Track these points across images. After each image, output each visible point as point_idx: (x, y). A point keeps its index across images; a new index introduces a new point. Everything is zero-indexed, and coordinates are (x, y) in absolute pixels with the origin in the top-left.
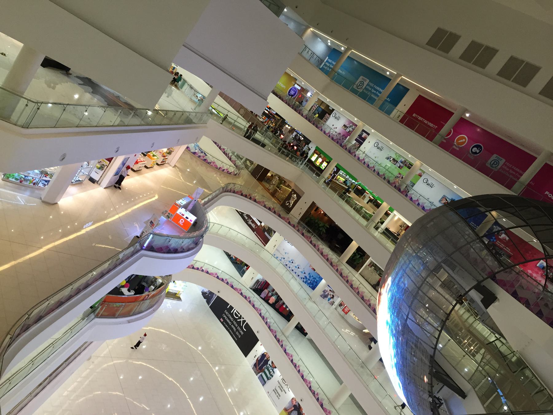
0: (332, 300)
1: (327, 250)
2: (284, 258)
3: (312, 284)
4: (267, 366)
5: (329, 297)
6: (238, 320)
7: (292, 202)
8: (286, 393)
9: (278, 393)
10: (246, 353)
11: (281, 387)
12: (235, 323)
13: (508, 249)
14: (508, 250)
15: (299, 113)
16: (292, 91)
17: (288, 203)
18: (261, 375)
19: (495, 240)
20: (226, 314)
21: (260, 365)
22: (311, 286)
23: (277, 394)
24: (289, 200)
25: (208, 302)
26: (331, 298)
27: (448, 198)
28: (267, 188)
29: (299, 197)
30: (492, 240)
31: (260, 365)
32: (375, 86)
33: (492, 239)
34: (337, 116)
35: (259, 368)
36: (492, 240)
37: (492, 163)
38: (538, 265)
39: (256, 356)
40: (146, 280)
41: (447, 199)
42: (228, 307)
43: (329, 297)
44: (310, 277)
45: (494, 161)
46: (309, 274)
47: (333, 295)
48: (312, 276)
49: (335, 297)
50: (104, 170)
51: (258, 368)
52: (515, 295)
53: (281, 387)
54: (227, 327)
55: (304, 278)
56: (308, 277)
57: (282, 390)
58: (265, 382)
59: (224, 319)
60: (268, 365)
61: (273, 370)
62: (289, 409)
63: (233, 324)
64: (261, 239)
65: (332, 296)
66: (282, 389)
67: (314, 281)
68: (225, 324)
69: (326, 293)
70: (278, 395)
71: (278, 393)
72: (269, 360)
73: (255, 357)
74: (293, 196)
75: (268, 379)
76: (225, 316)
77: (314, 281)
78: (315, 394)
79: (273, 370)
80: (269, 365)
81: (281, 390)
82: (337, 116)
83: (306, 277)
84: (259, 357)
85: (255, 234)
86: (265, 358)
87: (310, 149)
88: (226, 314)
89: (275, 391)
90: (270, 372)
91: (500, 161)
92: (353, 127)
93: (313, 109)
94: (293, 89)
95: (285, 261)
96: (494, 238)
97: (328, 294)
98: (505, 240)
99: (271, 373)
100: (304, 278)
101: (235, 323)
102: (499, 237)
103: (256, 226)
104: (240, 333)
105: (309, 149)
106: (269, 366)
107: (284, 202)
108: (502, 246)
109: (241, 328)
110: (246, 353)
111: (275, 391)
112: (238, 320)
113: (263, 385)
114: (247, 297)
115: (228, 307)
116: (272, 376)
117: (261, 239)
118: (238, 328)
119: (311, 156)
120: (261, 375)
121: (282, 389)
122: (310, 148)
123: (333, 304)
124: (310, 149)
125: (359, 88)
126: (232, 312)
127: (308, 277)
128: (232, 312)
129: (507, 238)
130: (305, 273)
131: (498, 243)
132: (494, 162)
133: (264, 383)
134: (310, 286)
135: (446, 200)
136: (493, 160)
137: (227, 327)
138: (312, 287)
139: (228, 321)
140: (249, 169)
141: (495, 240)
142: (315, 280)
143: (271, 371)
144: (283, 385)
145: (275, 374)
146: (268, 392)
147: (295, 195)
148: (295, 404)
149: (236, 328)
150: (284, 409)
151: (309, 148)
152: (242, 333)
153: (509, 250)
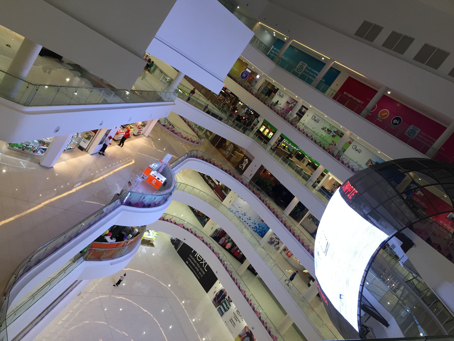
0: (277, 246)
1: (273, 205)
2: (238, 212)
3: (261, 233)
4: (224, 300)
5: (275, 243)
6: (201, 263)
7: (244, 165)
8: (240, 322)
9: (233, 322)
10: (207, 290)
11: (236, 318)
12: (198, 265)
13: (423, 203)
14: (423, 204)
15: (250, 92)
16: (244, 74)
17: (241, 166)
18: (220, 307)
19: (412, 196)
20: (190, 258)
21: (219, 299)
22: (260, 234)
23: (233, 323)
24: (242, 164)
25: (176, 248)
26: (277, 244)
27: (373, 161)
28: (224, 154)
29: (250, 161)
30: (410, 196)
31: (219, 299)
32: (427, 135)
33: (410, 195)
34: (281, 94)
35: (218, 302)
36: (410, 196)
37: (409, 132)
38: (448, 217)
39: (215, 292)
40: (125, 230)
41: (373, 162)
42: (192, 252)
43: (275, 243)
44: (259, 227)
45: (411, 130)
46: (259, 224)
47: (278, 242)
48: (261, 226)
49: (280, 244)
50: (91, 140)
51: (217, 301)
52: (429, 241)
53: (236, 318)
54: (192, 268)
55: (254, 228)
56: (258, 227)
57: (237, 320)
58: (223, 314)
59: (189, 261)
60: (225, 299)
61: (229, 304)
62: (242, 336)
63: (196, 265)
64: (219, 196)
65: (277, 243)
66: (236, 319)
67: (263, 230)
68: (190, 265)
69: (273, 240)
70: (234, 324)
71: (233, 322)
72: (226, 295)
73: (214, 293)
74: (245, 160)
75: (225, 311)
76: (190, 259)
77: (263, 230)
78: (264, 323)
79: (229, 304)
80: (226, 299)
81: (236, 320)
82: (281, 94)
83: (256, 227)
84: (218, 293)
85: (215, 192)
86: (223, 294)
87: (259, 122)
88: (190, 258)
89: (231, 320)
90: (227, 305)
91: (303, 66)
92: (295, 103)
93: (262, 89)
94: (245, 72)
95: (239, 214)
96: (411, 194)
97: (275, 240)
98: (421, 196)
99: (228, 306)
100: (254, 228)
101: (198, 265)
102: (416, 193)
103: (214, 185)
104: (202, 273)
105: (258, 122)
106: (226, 300)
107: (238, 166)
108: (418, 200)
109: (203, 269)
110: (207, 290)
111: (231, 320)
112: (201, 263)
113: (221, 316)
114: (208, 244)
115: (192, 252)
116: (229, 309)
117: (219, 196)
118: (201, 269)
119: (260, 128)
120: (220, 307)
121: (236, 319)
122: (259, 121)
123: (278, 249)
124: (259, 122)
125: (299, 71)
126: (195, 256)
127: (258, 227)
128: (195, 256)
129: (422, 195)
130: (255, 224)
131: (415, 198)
132: (300, 68)
133: (222, 314)
134: (259, 235)
135: (372, 163)
136: (411, 130)
137: (192, 268)
138: (261, 235)
139: (192, 263)
140: (210, 139)
141: (412, 196)
142: (264, 230)
143: (228, 304)
144: (238, 316)
145: (231, 307)
146: (226, 322)
147: (247, 160)
148: (248, 331)
149: (199, 269)
150: (238, 336)
151: (258, 121)
152: (204, 273)
153: (424, 204)
